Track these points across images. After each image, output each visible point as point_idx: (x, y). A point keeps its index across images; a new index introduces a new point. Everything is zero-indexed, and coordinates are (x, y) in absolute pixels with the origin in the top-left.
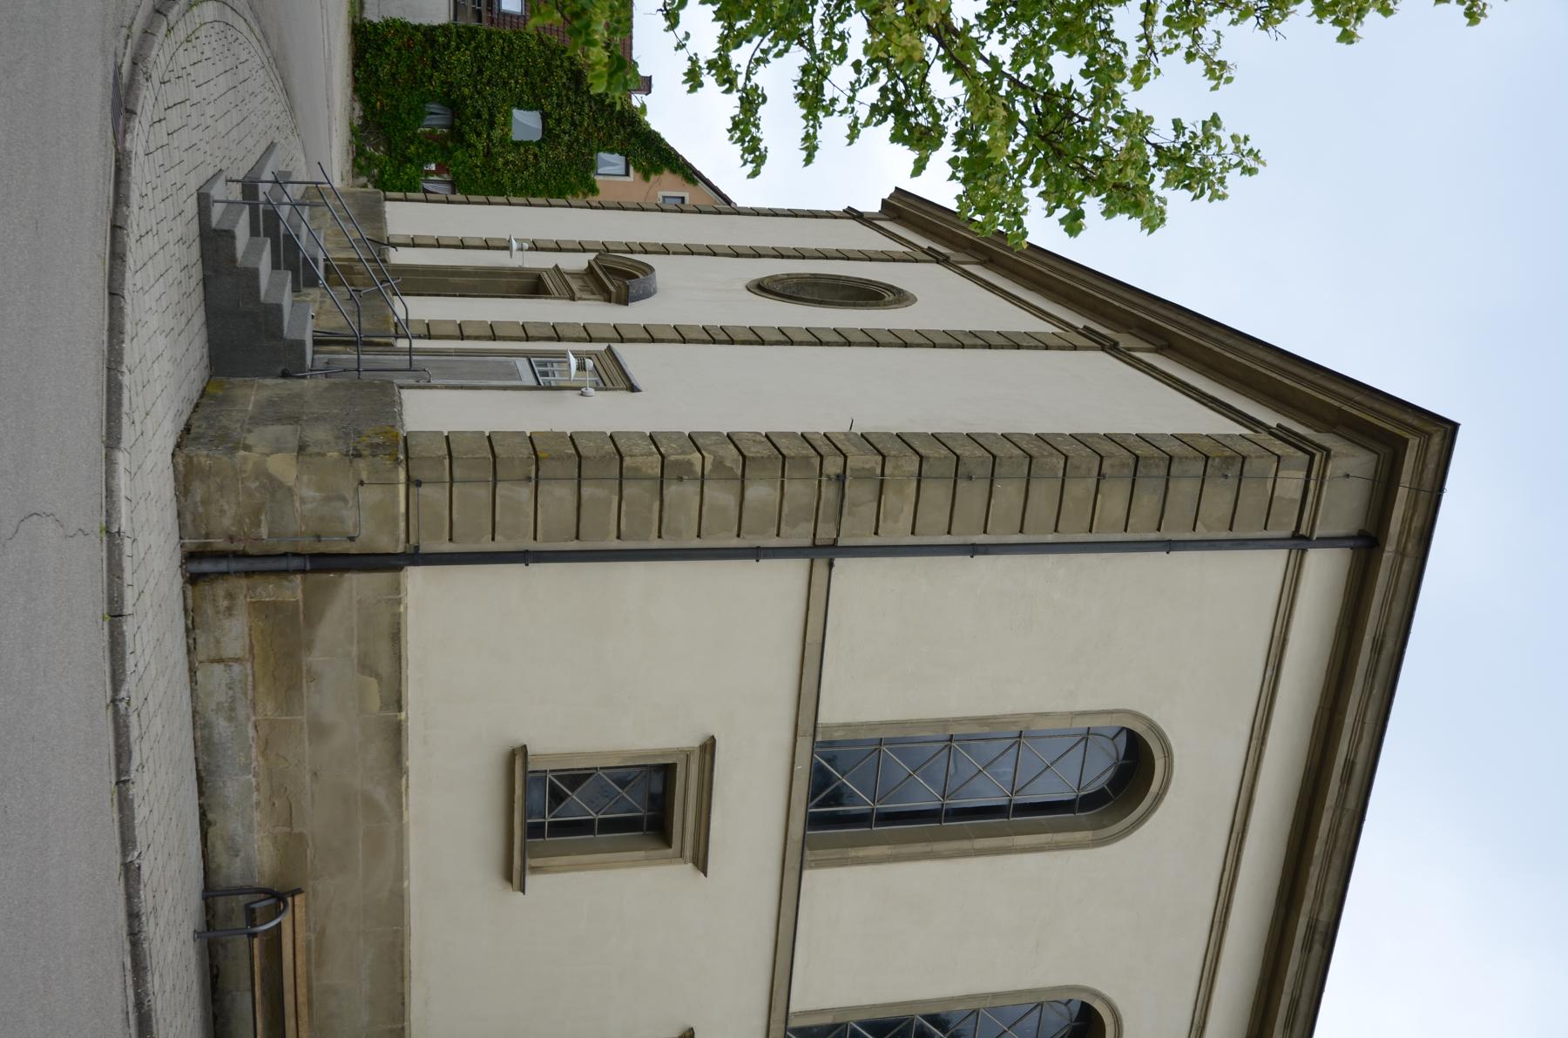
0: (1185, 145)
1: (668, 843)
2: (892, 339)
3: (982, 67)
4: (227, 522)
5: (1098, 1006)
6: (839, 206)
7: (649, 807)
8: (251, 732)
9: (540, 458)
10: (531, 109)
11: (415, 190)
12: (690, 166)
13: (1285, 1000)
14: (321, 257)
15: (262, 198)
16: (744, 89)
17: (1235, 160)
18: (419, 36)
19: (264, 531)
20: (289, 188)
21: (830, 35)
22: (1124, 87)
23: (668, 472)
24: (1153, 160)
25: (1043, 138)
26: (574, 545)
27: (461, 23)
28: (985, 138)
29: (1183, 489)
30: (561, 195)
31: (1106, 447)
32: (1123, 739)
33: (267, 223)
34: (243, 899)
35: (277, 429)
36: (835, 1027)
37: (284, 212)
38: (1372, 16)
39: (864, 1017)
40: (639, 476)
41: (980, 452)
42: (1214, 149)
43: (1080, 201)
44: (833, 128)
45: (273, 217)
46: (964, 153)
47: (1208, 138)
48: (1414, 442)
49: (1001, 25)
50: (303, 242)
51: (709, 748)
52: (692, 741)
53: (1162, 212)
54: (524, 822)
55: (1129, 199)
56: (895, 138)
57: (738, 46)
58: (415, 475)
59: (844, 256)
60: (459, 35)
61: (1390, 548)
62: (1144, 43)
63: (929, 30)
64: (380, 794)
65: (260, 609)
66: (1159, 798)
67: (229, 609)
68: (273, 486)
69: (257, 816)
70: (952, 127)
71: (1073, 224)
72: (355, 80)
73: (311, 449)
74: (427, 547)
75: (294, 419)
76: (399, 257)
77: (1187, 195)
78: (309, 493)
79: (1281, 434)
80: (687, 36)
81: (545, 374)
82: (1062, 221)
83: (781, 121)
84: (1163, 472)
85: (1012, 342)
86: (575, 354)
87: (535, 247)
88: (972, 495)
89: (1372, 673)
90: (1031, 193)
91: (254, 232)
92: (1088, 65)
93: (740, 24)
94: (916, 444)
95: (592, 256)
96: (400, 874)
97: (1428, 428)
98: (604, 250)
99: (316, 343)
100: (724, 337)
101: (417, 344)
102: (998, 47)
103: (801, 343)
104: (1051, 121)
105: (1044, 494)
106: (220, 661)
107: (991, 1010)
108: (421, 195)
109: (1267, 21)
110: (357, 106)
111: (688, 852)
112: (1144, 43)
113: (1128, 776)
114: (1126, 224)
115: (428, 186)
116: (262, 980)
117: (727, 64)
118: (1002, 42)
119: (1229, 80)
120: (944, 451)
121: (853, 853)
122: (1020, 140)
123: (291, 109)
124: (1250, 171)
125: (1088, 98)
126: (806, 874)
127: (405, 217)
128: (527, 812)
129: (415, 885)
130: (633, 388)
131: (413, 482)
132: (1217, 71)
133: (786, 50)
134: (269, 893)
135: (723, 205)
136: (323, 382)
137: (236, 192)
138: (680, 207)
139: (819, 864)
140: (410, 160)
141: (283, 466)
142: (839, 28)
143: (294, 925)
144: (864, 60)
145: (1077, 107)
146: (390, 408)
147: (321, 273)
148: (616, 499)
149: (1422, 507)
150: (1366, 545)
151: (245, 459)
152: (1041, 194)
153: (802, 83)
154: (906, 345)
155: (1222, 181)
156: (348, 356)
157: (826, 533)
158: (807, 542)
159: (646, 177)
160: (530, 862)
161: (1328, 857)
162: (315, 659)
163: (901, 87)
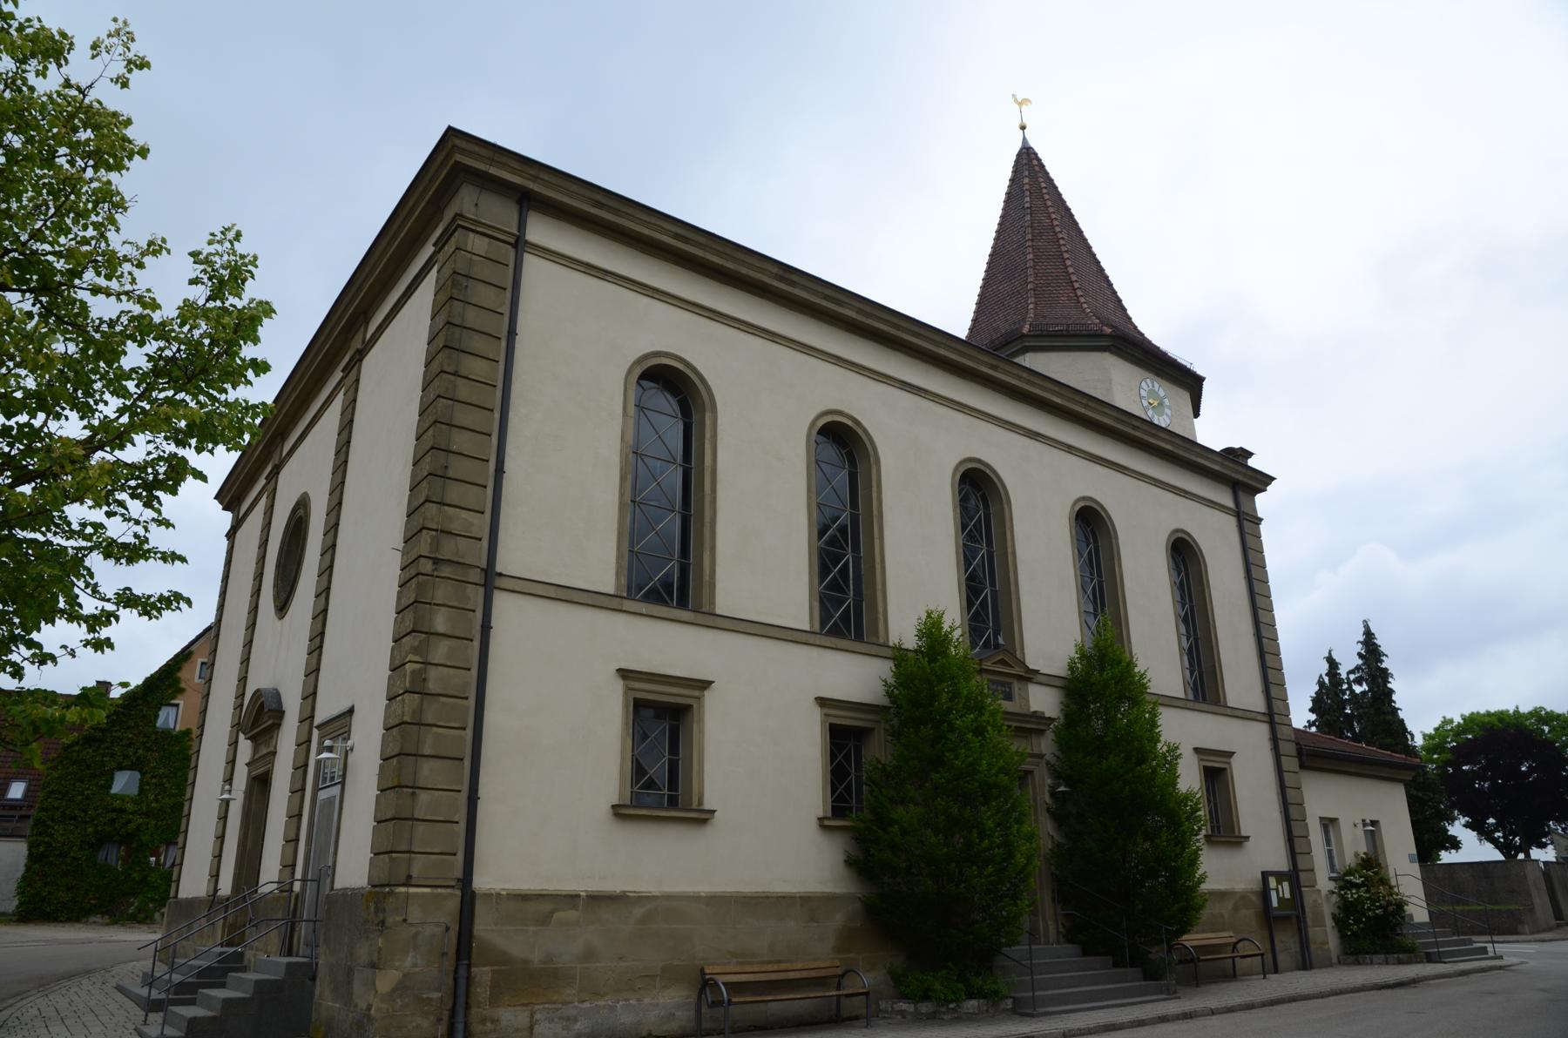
0: (210, 279)
1: (688, 708)
2: (334, 514)
3: (125, 419)
4: (426, 1023)
6: (225, 543)
7: (662, 724)
8: (587, 1005)
9: (398, 779)
10: (112, 779)
11: (171, 874)
12: (177, 656)
14: (219, 949)
15: (163, 996)
16: (117, 604)
17: (227, 244)
18: (36, 867)
19: (436, 995)
20: (157, 974)
21: (80, 534)
22: (157, 317)
23: (418, 688)
24: (219, 303)
25: (190, 380)
26: (467, 763)
27: (28, 832)
28: (183, 424)
29: (472, 317)
30: (188, 759)
31: (435, 366)
32: (644, 383)
33: (186, 992)
34: (704, 1009)
35: (357, 988)
36: (821, 601)
37: (177, 978)
38: (130, 132)
39: (816, 581)
40: (419, 711)
41: (428, 458)
42: (217, 258)
43: (243, 360)
44: (159, 538)
45: (181, 987)
46: (193, 442)
47: (207, 261)
48: (458, 157)
49: (91, 402)
50: (205, 964)
51: (624, 673)
52: (619, 685)
53: (261, 302)
54: (667, 809)
55: (248, 323)
56: (174, 492)
57: (80, 606)
58: (402, 879)
59: (264, 544)
60: (40, 834)
61: (531, 185)
62: (123, 298)
63: (87, 457)
64: (638, 912)
65: (495, 999)
67: (493, 1021)
68: (401, 988)
69: (647, 1000)
70: (171, 448)
71: (261, 367)
72: (69, 920)
73: (375, 958)
74: (458, 872)
75: (350, 971)
76: (225, 887)
77: (250, 282)
78: (409, 961)
79: (440, 245)
80: (64, 647)
81: (332, 778)
82: (257, 375)
83: (148, 578)
84: (457, 330)
85: (347, 426)
86: (319, 753)
87: (229, 780)
88: (458, 467)
89: (616, 212)
90: (232, 395)
91: (192, 1002)
92: (135, 341)
93: (62, 605)
94: (416, 504)
95: (241, 736)
96: (695, 898)
97: (449, 146)
98: (238, 727)
99: (290, 954)
100: (318, 640)
101: (298, 875)
102: (110, 406)
103: (330, 582)
104: (177, 373)
105: (464, 416)
106: (531, 1028)
107: (818, 494)
108: (176, 870)
109: (121, 206)
110: (92, 919)
111: (697, 693)
112: (123, 298)
113: (670, 385)
114: (266, 329)
115: (169, 864)
117: (94, 616)
118: (106, 403)
119: (164, 240)
120: (424, 484)
121: (707, 578)
122: (188, 398)
123: (87, 972)
124: (238, 235)
125: (162, 344)
126: (718, 611)
127: (193, 883)
128: (660, 807)
129: (704, 888)
130: (351, 711)
131: (408, 883)
132: (155, 248)
133: (89, 570)
134: (702, 991)
135: (211, 634)
136: (322, 948)
137: (157, 1018)
138: (209, 666)
139: (712, 602)
140: (145, 877)
141: (386, 981)
142: (75, 527)
143: (726, 973)
144: (105, 508)
145: (168, 353)
146: (349, 896)
147: (232, 950)
148: (435, 729)
149: (504, 159)
150: (527, 201)
151: (378, 1009)
152: (234, 388)
153: (118, 560)
154: (340, 504)
155: (242, 257)
156: (303, 930)
157: (476, 576)
158: (481, 590)
159: (182, 691)
160: (695, 806)
161: (735, 260)
162: (536, 957)
163: (133, 483)
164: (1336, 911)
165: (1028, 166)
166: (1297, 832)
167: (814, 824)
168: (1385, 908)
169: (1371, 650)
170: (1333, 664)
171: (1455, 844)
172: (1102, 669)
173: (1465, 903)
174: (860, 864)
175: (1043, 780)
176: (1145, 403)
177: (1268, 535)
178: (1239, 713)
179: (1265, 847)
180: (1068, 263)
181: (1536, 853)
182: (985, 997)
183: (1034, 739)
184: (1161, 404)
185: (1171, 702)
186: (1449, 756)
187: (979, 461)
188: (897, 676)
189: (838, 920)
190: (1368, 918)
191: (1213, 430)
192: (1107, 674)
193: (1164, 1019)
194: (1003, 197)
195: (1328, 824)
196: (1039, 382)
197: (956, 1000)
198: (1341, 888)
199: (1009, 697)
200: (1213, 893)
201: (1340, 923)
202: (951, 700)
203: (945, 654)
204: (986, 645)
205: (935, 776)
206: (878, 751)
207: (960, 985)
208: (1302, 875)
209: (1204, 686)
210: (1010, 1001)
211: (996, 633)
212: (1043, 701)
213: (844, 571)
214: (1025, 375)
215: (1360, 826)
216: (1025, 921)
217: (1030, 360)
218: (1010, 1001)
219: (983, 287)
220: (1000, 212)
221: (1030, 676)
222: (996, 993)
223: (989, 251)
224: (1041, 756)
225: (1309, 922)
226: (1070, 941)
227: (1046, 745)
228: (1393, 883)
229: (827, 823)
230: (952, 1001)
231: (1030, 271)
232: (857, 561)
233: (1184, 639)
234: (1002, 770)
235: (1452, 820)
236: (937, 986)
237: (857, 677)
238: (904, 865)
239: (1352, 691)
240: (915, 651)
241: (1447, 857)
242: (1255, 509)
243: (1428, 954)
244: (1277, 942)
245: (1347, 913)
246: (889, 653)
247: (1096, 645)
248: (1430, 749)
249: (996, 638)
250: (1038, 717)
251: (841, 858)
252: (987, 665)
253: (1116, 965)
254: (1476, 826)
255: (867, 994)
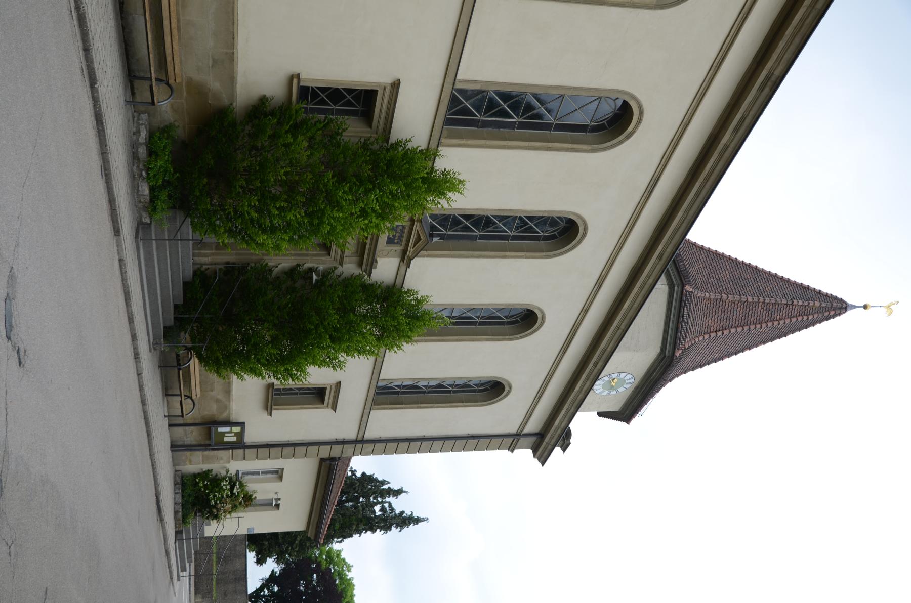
5: (536, 311)
13: (738, 116)
66: (628, 137)
107: (571, 96)
113: (616, 121)
116: (150, 10)
161: (793, 36)
164: (214, 473)
165: (830, 307)
166: (274, 451)
167: (296, 70)
168: (215, 507)
169: (405, 521)
170: (397, 493)
171: (260, 561)
172: (406, 316)
173: (217, 564)
174: (260, 109)
175: (322, 263)
176: (614, 376)
177: (502, 456)
178: (365, 418)
179: (261, 426)
180: (739, 329)
182: (151, 201)
183: (355, 259)
184: (612, 388)
185: (377, 368)
186: (324, 565)
187: (584, 236)
188: (413, 151)
189: (214, 84)
190: (208, 495)
191: (584, 423)
192: (403, 320)
193: (134, 337)
194: (806, 283)
195: (279, 474)
196: (643, 292)
197: (148, 178)
198: (230, 478)
199: (390, 241)
200: (229, 385)
201: (205, 475)
202: (391, 193)
203: (429, 191)
204: (433, 228)
205: (330, 174)
206: (353, 130)
207: (160, 182)
208: (241, 451)
209: (387, 395)
210: (148, 220)
211: (442, 237)
212: (385, 269)
213: (505, 114)
214: (651, 281)
215: (276, 497)
216: (211, 239)
217: (662, 287)
218: (148, 220)
219: (729, 258)
220: (793, 279)
221: (405, 259)
222: (155, 209)
223: (760, 266)
224: (341, 263)
225: (206, 453)
226: (195, 273)
227: (350, 268)
228: (233, 515)
229: (295, 81)
230: (148, 174)
231: (737, 298)
232: (511, 126)
233: (425, 383)
234: (333, 228)
235: (278, 561)
236: (160, 163)
237: (414, 118)
238: (259, 145)
239: (376, 504)
240: (432, 168)
241: (251, 557)
242: (521, 447)
243: (181, 532)
244: (192, 428)
245: (214, 481)
246: (433, 145)
247: (425, 313)
248: (329, 553)
249: (438, 235)
250: (372, 263)
251: (268, 93)
252: (417, 226)
253: (176, 307)
254: (273, 578)
255: (153, 103)
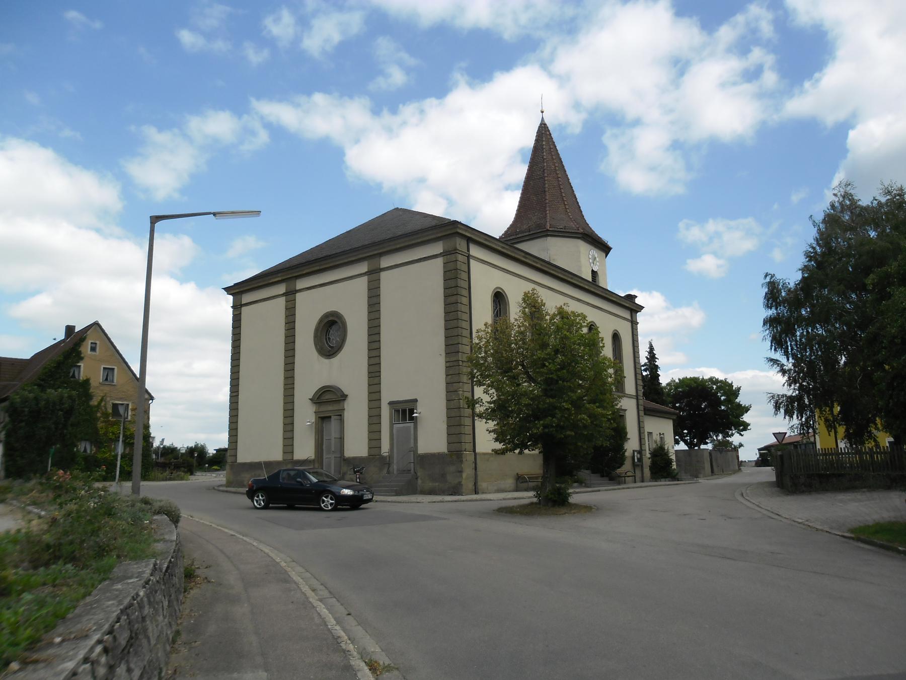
150: (469, 240)
177: (640, 328)
181: (702, 447)
195: (650, 434)
